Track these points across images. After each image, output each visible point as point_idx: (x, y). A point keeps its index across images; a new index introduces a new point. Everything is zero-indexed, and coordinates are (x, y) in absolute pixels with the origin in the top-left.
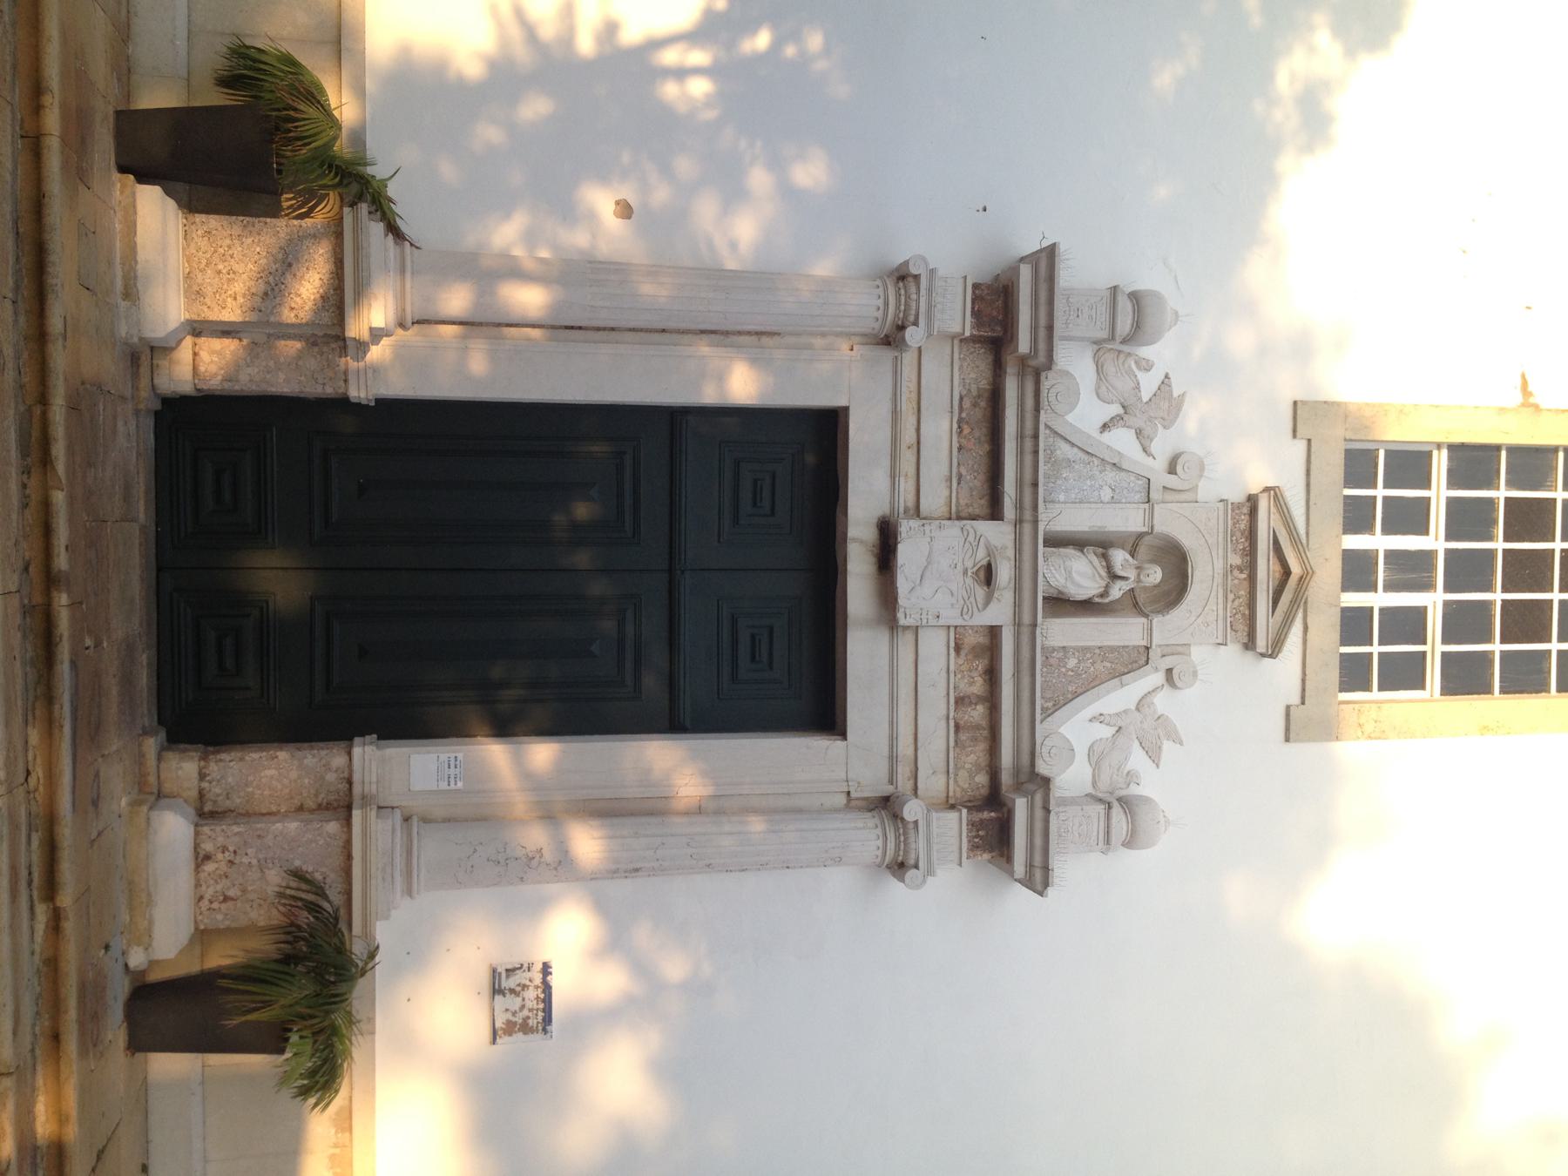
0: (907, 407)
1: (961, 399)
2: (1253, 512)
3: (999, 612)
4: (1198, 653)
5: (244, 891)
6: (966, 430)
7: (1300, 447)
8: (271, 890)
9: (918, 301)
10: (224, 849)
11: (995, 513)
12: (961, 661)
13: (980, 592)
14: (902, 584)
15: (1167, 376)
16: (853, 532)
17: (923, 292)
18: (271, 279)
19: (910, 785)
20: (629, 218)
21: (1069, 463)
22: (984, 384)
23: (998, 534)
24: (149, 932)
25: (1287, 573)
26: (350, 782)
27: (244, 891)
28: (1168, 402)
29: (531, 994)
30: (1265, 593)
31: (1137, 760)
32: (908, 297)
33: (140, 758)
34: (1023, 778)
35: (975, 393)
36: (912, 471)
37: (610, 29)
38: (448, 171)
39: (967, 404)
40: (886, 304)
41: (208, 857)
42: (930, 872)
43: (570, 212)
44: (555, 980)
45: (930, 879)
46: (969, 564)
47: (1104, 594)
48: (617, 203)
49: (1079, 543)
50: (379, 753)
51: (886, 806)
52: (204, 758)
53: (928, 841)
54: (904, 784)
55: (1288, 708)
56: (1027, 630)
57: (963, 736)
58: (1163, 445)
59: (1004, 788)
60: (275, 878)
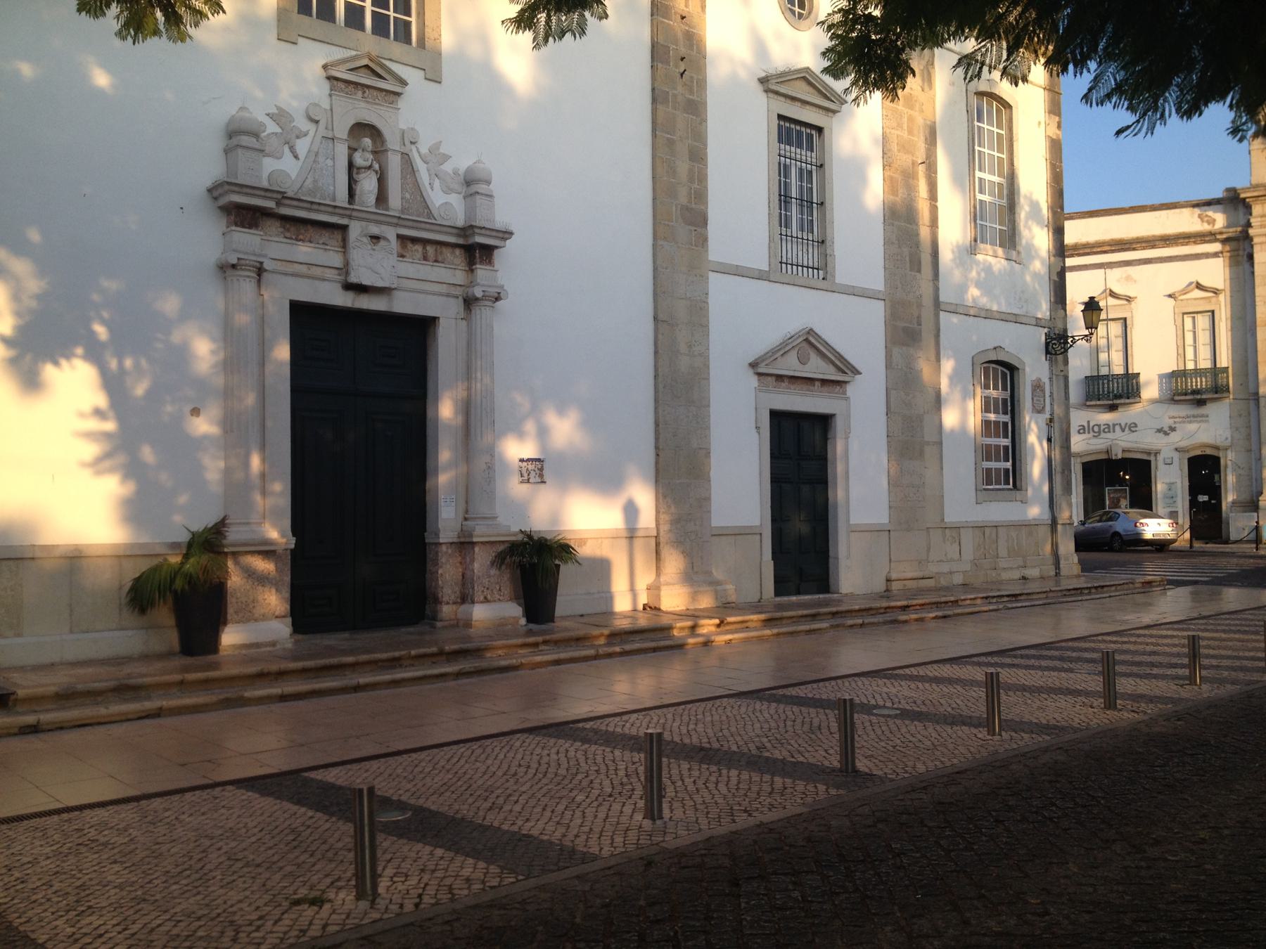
0: (290, 268)
1: (286, 238)
2: (337, 79)
3: (391, 233)
4: (403, 126)
5: (498, 583)
6: (301, 237)
7: (301, 40)
8: (497, 572)
9: (250, 260)
10: (483, 591)
11: (344, 228)
12: (408, 255)
13: (382, 243)
14: (380, 284)
15: (268, 115)
16: (349, 304)
17: (246, 257)
18: (256, 584)
19: (458, 288)
20: (199, 409)
21: (315, 181)
22: (278, 224)
23: (355, 229)
24: (514, 618)
25: (367, 66)
26: (451, 543)
27: (498, 583)
28: (280, 116)
29: (530, 467)
30: (379, 83)
31: (448, 167)
32: (246, 265)
33: (445, 627)
34: (462, 233)
35: (282, 230)
36: (321, 269)
37: (98, 413)
38: (183, 499)
39: (288, 235)
40: (248, 277)
41: (485, 598)
42: (502, 287)
43: (200, 443)
44: (526, 457)
45: (505, 288)
46: (369, 247)
47: (376, 172)
48: (192, 415)
49: (352, 182)
50: (441, 532)
51: (469, 302)
52: (441, 603)
53: (490, 286)
54: (458, 291)
55: (426, 79)
56: (399, 221)
57: (440, 259)
58: (304, 125)
59: (465, 243)
60: (493, 572)
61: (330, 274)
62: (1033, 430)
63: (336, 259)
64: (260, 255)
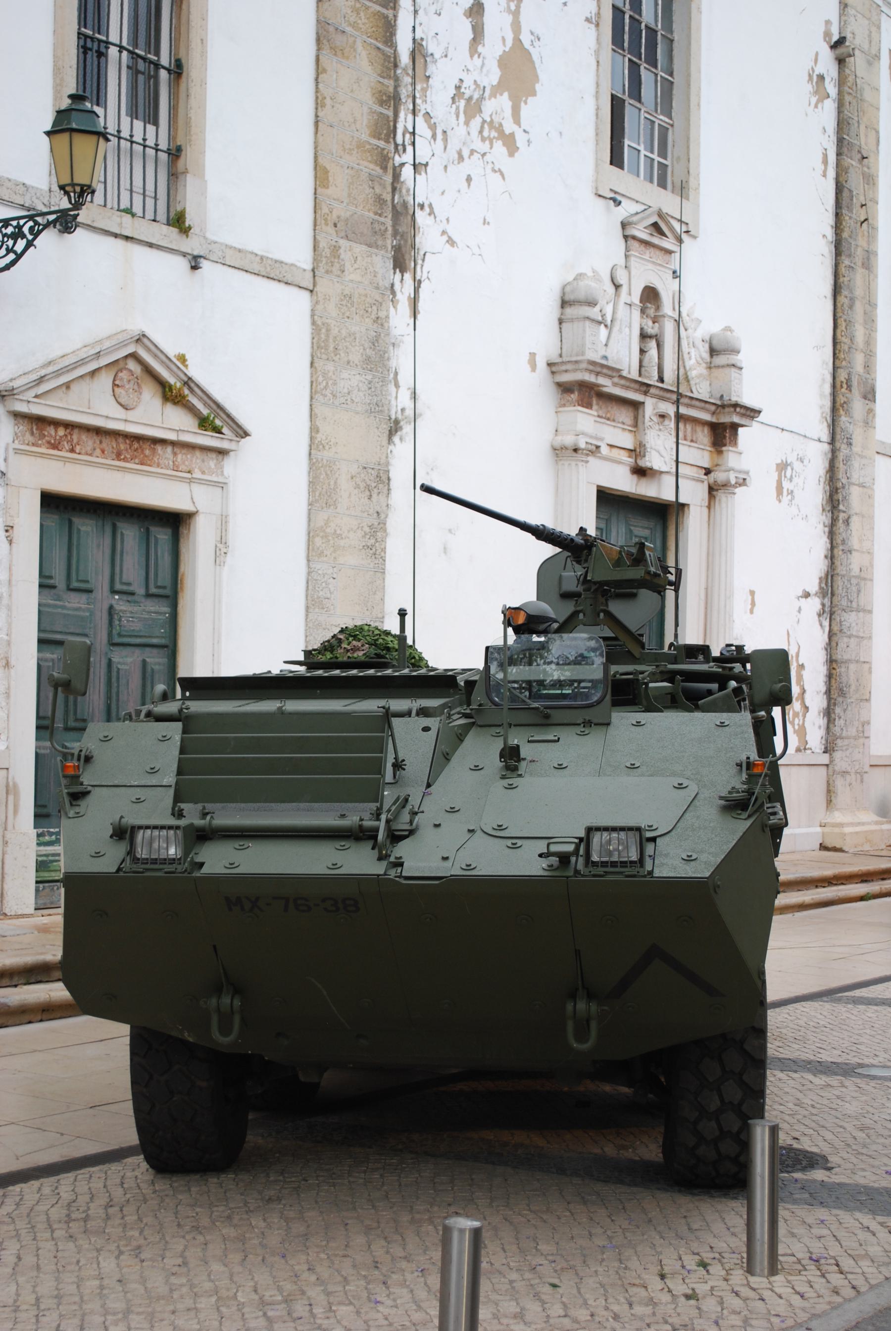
11: (636, 406)
61: (624, 456)
62: (280, 708)
63: (627, 441)
64: (597, 438)
